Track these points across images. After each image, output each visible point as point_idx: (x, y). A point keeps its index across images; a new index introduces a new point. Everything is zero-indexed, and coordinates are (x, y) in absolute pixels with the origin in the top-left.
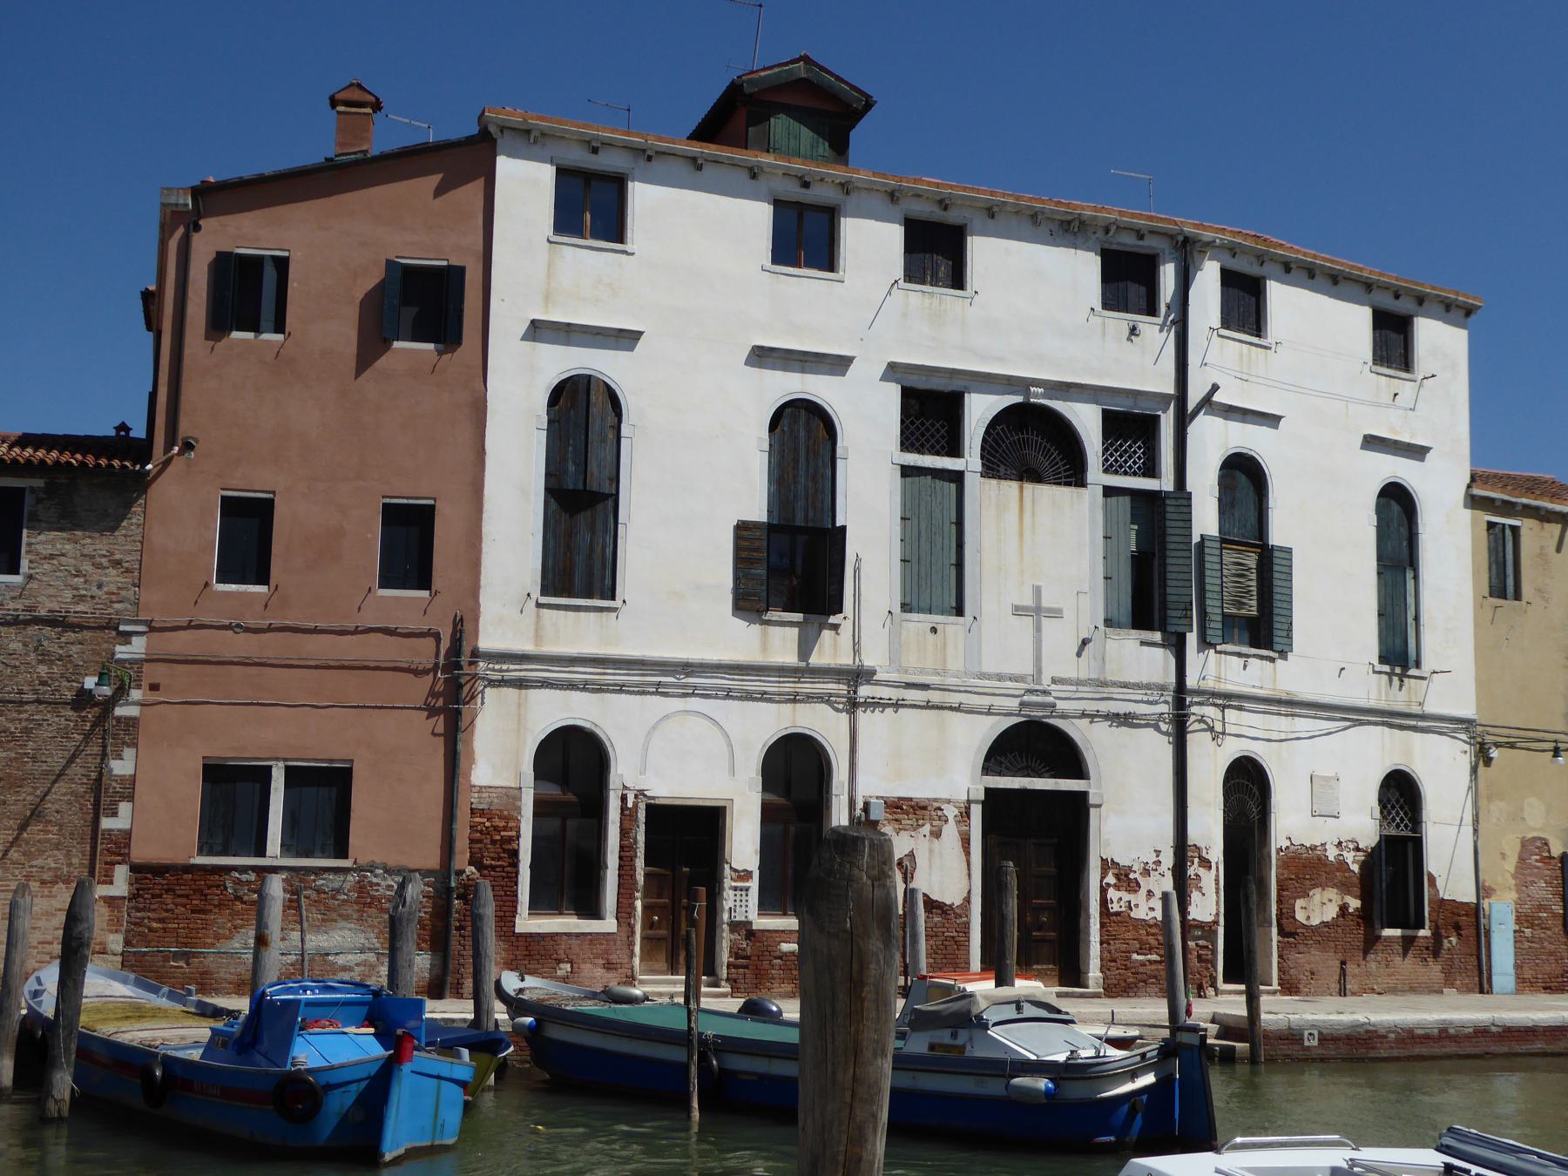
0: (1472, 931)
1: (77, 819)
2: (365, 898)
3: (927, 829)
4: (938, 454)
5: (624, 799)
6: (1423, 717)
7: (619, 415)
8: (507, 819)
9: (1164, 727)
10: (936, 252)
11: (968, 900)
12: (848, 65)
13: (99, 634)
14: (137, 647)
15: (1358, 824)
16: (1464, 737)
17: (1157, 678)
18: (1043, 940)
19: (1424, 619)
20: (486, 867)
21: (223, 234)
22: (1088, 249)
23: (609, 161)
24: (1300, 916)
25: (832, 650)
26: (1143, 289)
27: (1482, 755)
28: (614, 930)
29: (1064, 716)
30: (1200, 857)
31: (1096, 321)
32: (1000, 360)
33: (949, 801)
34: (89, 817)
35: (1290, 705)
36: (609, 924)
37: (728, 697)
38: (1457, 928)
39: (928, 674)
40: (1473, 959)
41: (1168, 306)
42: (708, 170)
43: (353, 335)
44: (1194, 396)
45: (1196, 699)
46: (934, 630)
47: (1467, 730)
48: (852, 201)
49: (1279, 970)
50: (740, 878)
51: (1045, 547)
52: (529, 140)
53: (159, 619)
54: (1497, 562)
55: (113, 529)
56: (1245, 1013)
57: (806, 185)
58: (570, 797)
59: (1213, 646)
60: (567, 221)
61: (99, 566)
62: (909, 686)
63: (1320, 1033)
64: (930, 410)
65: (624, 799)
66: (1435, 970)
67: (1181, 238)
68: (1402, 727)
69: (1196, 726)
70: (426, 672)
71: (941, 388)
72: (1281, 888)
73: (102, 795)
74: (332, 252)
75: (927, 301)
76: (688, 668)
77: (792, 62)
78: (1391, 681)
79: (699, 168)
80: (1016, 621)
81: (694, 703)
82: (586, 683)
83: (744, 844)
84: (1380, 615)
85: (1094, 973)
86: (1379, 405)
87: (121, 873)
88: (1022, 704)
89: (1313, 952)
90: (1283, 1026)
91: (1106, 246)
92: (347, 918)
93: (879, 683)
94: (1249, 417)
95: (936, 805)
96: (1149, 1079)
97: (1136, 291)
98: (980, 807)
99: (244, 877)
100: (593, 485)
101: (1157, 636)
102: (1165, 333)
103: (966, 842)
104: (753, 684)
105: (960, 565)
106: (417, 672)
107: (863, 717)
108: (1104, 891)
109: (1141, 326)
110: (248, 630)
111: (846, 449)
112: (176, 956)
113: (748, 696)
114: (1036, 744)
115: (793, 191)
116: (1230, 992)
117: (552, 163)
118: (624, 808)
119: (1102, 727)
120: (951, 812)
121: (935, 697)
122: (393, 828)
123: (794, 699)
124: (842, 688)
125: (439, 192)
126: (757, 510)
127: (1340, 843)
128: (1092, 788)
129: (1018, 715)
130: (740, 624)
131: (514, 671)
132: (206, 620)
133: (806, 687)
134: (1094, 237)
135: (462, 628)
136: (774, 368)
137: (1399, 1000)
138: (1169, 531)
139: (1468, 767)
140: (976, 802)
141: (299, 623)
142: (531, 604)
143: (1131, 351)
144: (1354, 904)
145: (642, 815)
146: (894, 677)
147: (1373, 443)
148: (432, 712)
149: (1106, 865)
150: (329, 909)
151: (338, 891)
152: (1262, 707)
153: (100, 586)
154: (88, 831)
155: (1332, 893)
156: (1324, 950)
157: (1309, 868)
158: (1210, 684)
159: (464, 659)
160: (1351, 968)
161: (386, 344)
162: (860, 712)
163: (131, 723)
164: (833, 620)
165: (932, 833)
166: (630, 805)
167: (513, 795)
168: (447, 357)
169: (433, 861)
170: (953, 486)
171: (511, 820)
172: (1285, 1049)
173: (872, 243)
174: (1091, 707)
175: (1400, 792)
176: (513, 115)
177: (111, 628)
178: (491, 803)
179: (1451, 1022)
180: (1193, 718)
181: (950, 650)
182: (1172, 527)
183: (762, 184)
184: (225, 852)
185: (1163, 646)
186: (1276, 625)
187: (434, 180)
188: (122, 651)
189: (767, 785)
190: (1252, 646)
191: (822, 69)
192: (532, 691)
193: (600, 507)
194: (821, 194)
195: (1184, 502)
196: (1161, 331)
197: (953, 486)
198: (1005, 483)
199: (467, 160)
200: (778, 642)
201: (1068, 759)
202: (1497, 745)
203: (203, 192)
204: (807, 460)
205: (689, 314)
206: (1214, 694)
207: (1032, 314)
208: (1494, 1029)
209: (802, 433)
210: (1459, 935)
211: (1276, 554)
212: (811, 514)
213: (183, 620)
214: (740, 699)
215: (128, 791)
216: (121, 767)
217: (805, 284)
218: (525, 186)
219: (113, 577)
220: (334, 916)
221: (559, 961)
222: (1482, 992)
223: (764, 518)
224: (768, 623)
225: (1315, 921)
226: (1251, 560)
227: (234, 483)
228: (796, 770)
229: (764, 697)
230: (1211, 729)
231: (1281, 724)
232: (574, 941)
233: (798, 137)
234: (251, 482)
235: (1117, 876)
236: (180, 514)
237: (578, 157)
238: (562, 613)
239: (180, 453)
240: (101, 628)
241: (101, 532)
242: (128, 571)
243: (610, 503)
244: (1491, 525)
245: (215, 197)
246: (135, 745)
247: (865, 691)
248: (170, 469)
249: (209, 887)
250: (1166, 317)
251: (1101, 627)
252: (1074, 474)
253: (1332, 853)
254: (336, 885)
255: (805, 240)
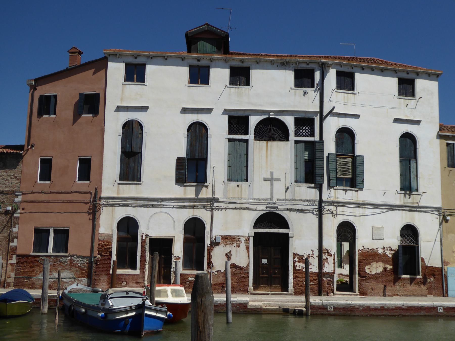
0: (440, 276)
1: (5, 243)
2: (72, 264)
3: (235, 244)
4: (241, 134)
5: (142, 236)
6: (419, 207)
7: (142, 130)
8: (108, 242)
9: (315, 213)
10: (240, 76)
11: (248, 265)
12: (219, 24)
13: (11, 196)
14: (19, 199)
15: (392, 241)
16: (437, 213)
17: (313, 198)
18: (262, 277)
19: (419, 175)
20: (103, 256)
21: (46, 90)
22: (290, 70)
23: (140, 60)
24: (367, 271)
25: (205, 193)
26: (310, 80)
27: (444, 219)
28: (139, 273)
29: (281, 210)
30: (328, 253)
31: (292, 91)
32: (261, 105)
33: (242, 236)
34: (8, 243)
35: (364, 205)
36: (138, 272)
37: (173, 207)
38: (434, 275)
39: (236, 199)
40: (441, 286)
41: (317, 84)
42: (169, 59)
43: (72, 114)
44: (325, 112)
45: (326, 204)
46: (238, 186)
47: (438, 211)
48: (213, 64)
49: (359, 288)
50: (177, 259)
51: (275, 161)
52: (117, 57)
53: (25, 191)
54: (451, 156)
55: (15, 168)
56: (225, 299)
57: (199, 60)
58: (129, 236)
59: (333, 187)
60: (129, 78)
61: (11, 178)
62: (230, 203)
63: (334, 307)
64: (238, 122)
65: (142, 236)
66: (424, 289)
67: (321, 63)
68: (410, 211)
69: (327, 212)
70: (88, 203)
71: (241, 115)
72: (360, 262)
73: (11, 237)
74: (66, 93)
75: (237, 90)
76: (162, 200)
77: (203, 26)
78: (405, 196)
79: (166, 59)
80: (265, 183)
81: (163, 210)
82: (131, 205)
83: (178, 249)
84: (401, 175)
85: (291, 287)
86: (400, 108)
87: (14, 257)
88: (267, 207)
89: (373, 282)
90: (321, 304)
91: (296, 68)
92: (67, 269)
93: (220, 202)
94: (347, 116)
95: (238, 237)
96: (133, 314)
97: (307, 81)
98: (253, 238)
99: (43, 258)
100: (134, 150)
101: (313, 185)
102: (316, 93)
103: (248, 248)
104: (181, 204)
105: (247, 167)
106: (86, 203)
107: (215, 212)
108: (294, 263)
109: (308, 91)
110: (45, 193)
111: (211, 135)
112: (27, 279)
113: (180, 207)
114: (271, 219)
115: (195, 63)
116: (339, 294)
117: (123, 62)
118: (142, 239)
119: (294, 214)
120: (243, 239)
121: (238, 206)
122: (79, 245)
123: (194, 208)
124: (209, 204)
125: (94, 73)
126: (183, 154)
127: (384, 248)
128: (290, 232)
129: (266, 210)
130: (178, 187)
131: (111, 202)
132: (35, 191)
133: (197, 204)
134: (292, 66)
135: (97, 190)
136: (189, 114)
137: (412, 298)
138: (317, 153)
139: (438, 223)
140: (251, 236)
141: (57, 191)
142: (116, 184)
143: (305, 100)
144: (390, 267)
145: (148, 241)
146: (225, 200)
147: (397, 121)
148: (89, 213)
149: (295, 255)
150: (63, 267)
151: (65, 262)
152: (352, 206)
153: (11, 183)
154: (7, 246)
155: (381, 264)
156: (377, 282)
157: (371, 256)
158: (332, 199)
159: (97, 199)
160: (388, 288)
161: (80, 115)
162: (214, 211)
163: (17, 218)
164: (206, 184)
165: (237, 246)
166: (144, 238)
167: (110, 236)
168: (95, 118)
169: (88, 254)
170: (245, 144)
171: (109, 243)
172: (321, 311)
173: (220, 75)
174: (289, 207)
175: (410, 232)
176: (112, 51)
177: (14, 194)
178: (104, 238)
179: (385, 305)
180: (325, 210)
181: (243, 192)
182: (318, 152)
183: (186, 61)
184: (39, 252)
185: (315, 188)
186: (358, 180)
187: (93, 70)
188: (16, 200)
189: (185, 232)
190: (351, 187)
191: (212, 26)
192: (116, 208)
193: (137, 156)
194: (204, 63)
195: (321, 144)
196: (315, 92)
197: (245, 144)
198: (262, 142)
199: (100, 65)
200: (189, 192)
201: (284, 224)
202: (450, 215)
203: (35, 80)
204: (199, 139)
205: (164, 101)
206: (333, 202)
207: (273, 90)
208: (404, 307)
209: (198, 132)
210: (435, 277)
211: (358, 158)
212: (200, 155)
213: (30, 191)
214: (177, 208)
215: (16, 235)
216: (15, 230)
217: (200, 89)
218: (116, 70)
219: (14, 181)
220: (64, 268)
221: (123, 282)
222: (444, 296)
223: (185, 156)
224: (186, 186)
225: (374, 272)
226: (350, 160)
227: (43, 155)
228: (194, 229)
229: (184, 207)
230: (332, 213)
231: (361, 211)
232: (127, 276)
233: (206, 47)
234: (47, 155)
235: (299, 258)
236: (32, 164)
237: (131, 60)
238: (125, 186)
239: (31, 148)
240: (11, 194)
241: (12, 169)
242: (18, 179)
243: (140, 154)
244: (448, 144)
245: (40, 81)
246: (18, 224)
247: (215, 205)
248: (29, 152)
249: (35, 261)
250: (316, 88)
251: (293, 183)
252: (285, 137)
253: (381, 251)
254: (65, 260)
255: (199, 76)
